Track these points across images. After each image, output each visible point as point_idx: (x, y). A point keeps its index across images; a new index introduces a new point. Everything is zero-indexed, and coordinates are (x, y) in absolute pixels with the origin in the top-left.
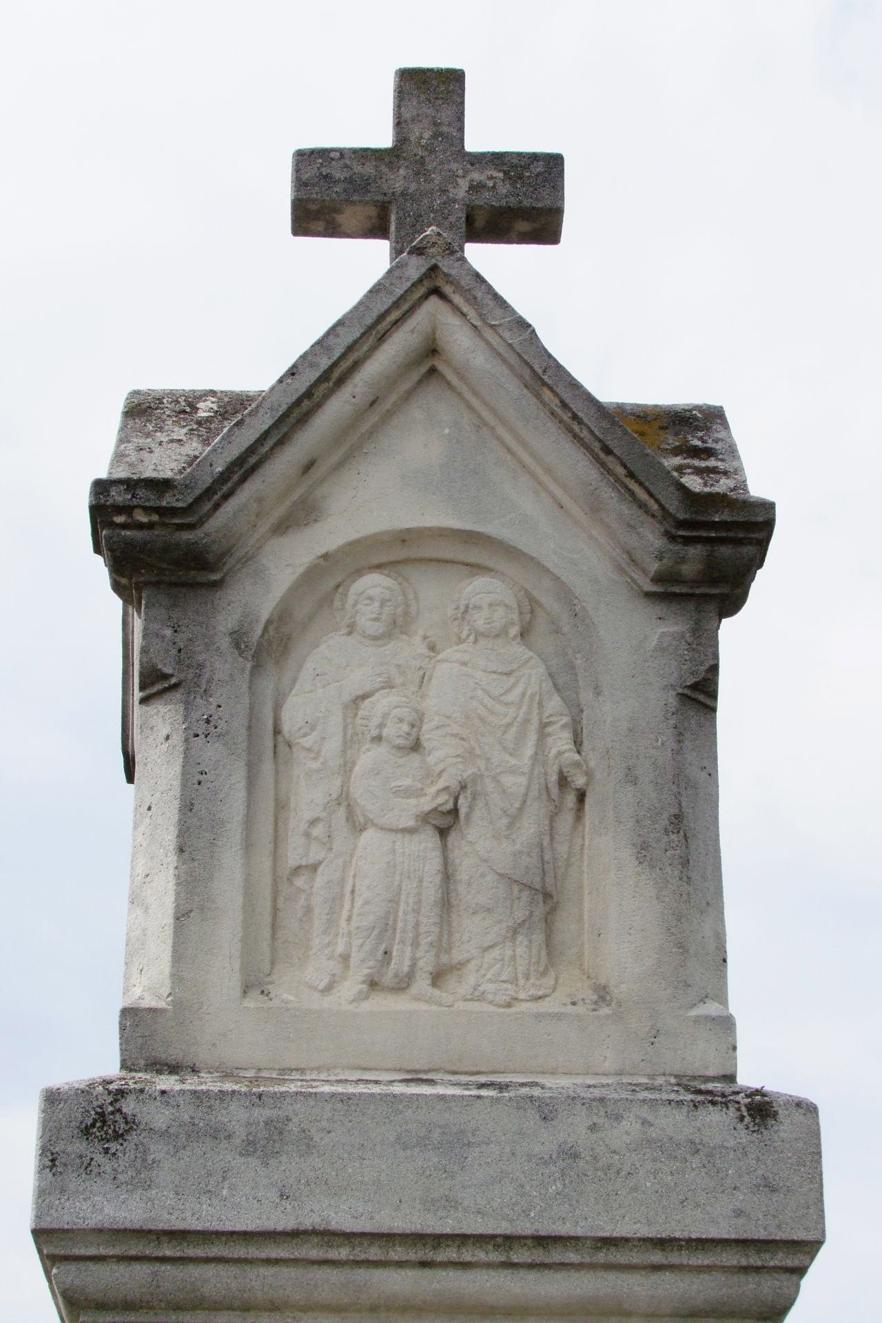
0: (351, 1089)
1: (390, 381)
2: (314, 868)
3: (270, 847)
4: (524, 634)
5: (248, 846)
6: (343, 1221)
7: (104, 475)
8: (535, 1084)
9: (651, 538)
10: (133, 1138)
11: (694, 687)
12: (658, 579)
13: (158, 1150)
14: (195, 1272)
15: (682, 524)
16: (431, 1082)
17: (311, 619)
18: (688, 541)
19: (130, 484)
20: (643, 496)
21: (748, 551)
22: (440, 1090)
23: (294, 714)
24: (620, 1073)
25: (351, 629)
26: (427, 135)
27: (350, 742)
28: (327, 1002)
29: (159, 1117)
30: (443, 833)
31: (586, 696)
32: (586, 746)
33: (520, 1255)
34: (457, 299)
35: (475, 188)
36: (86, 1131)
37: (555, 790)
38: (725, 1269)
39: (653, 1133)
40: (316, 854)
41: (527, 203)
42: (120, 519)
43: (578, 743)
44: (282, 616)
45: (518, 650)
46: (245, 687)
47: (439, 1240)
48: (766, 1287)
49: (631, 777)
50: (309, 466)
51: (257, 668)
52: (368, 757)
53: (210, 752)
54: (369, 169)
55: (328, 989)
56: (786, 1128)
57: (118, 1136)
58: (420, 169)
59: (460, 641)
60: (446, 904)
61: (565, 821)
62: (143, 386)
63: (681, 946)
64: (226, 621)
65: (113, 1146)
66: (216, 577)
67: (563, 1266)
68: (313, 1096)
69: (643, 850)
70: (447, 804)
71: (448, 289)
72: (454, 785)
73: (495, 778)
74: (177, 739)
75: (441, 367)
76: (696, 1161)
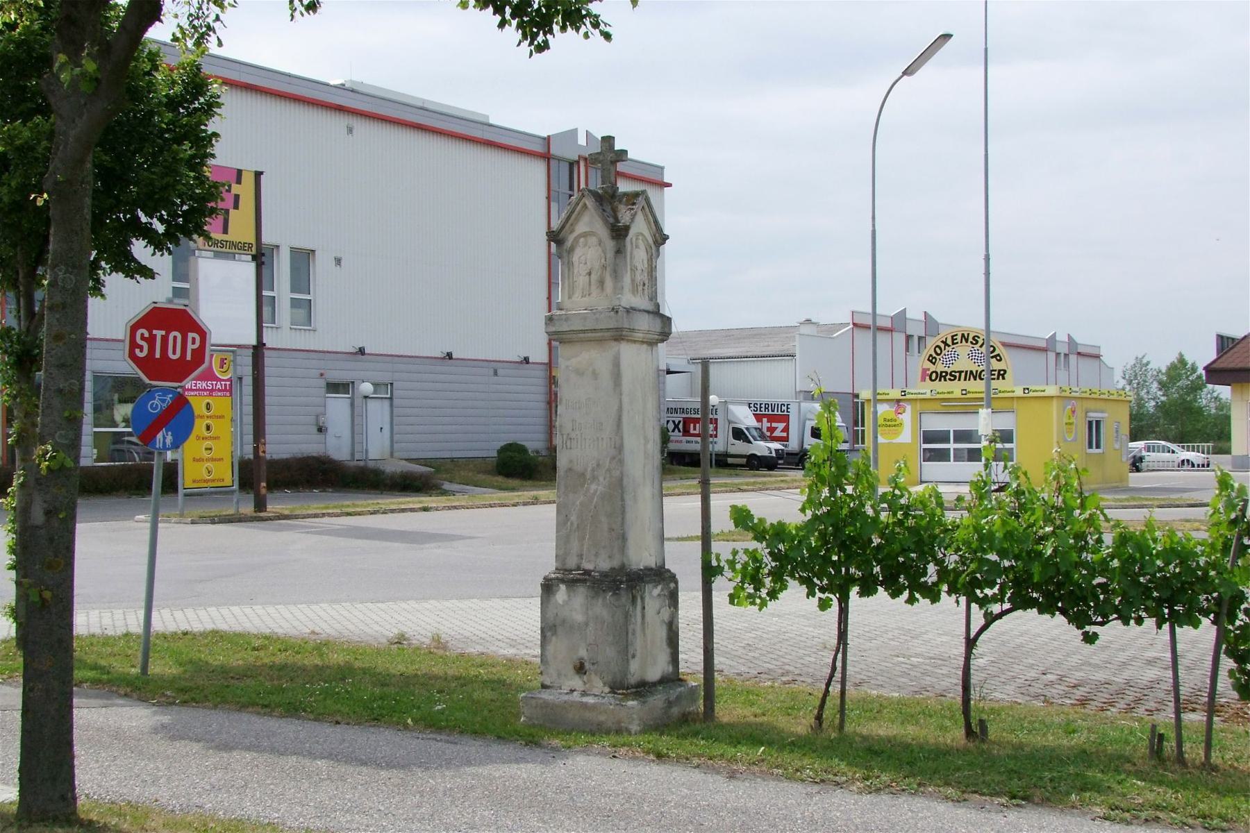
29: (556, 318)
64: (565, 248)
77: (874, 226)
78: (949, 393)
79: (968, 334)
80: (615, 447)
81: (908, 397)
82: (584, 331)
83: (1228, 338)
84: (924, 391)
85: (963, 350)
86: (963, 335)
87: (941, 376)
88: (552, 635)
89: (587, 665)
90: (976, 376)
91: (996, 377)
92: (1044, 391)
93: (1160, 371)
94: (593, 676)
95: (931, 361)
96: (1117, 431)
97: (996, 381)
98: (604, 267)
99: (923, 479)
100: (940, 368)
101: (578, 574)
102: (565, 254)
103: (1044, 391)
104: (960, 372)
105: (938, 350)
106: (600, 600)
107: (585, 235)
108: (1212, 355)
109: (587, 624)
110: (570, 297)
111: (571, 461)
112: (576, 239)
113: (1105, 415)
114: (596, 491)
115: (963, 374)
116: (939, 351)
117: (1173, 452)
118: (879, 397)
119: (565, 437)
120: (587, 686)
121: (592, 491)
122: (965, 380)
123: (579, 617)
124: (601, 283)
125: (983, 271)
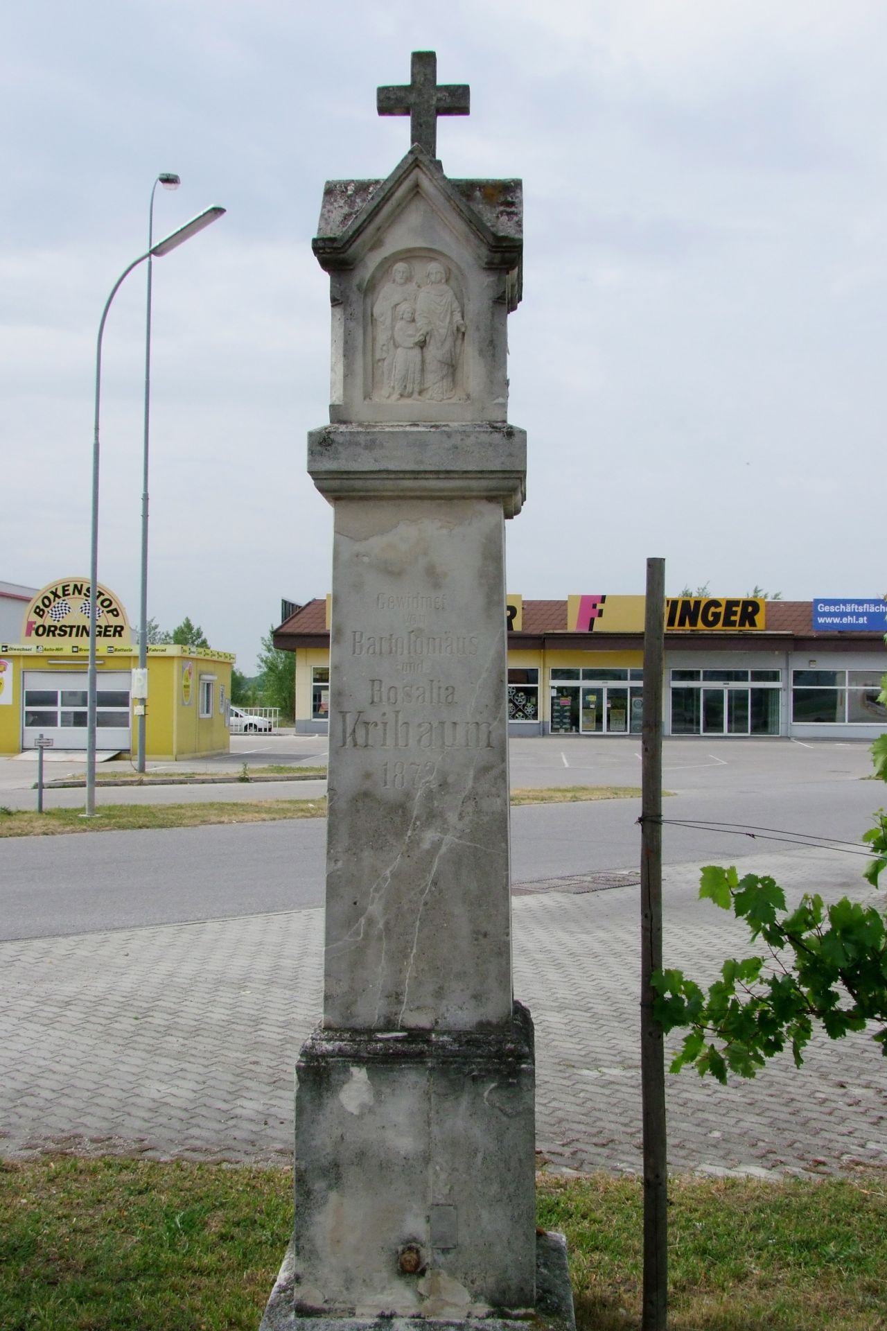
0: (397, 429)
1: (404, 197)
2: (384, 360)
3: (371, 353)
4: (447, 281)
5: (364, 353)
6: (392, 467)
7: (315, 236)
8: (447, 425)
9: (484, 251)
10: (334, 445)
11: (499, 298)
13: (340, 449)
14: (352, 482)
15: (493, 247)
16: (417, 425)
17: (382, 277)
18: (496, 252)
19: (323, 240)
20: (481, 236)
21: (515, 255)
22: (419, 429)
23: (377, 310)
24: (473, 420)
25: (394, 281)
26: (422, 79)
27: (394, 320)
28: (389, 401)
29: (340, 439)
30: (422, 348)
31: (466, 301)
32: (465, 318)
33: (442, 476)
34: (424, 169)
35: (439, 100)
36: (320, 444)
37: (455, 332)
38: (499, 478)
39: (479, 441)
40: (384, 355)
41: (456, 105)
42: (321, 251)
43: (463, 317)
44: (373, 277)
45: (445, 287)
46: (361, 303)
47: (419, 472)
48: (511, 483)
49: (478, 329)
50: (379, 229)
51: (365, 296)
53: (352, 324)
54: (402, 94)
55: (389, 397)
56: (516, 439)
57: (329, 445)
58: (420, 94)
59: (428, 284)
60: (423, 370)
61: (459, 342)
62: (330, 179)
63: (492, 382)
64: (356, 281)
65: (328, 448)
66: (351, 267)
67: (454, 478)
69: (481, 352)
70: (422, 338)
71: (421, 165)
72: (425, 333)
73: (437, 331)
74: (342, 320)
75: (420, 190)
76: (491, 448)
77: (97, 438)
78: (57, 649)
79: (82, 585)
80: (489, 745)
81: (10, 653)
82: (415, 474)
83: (290, 604)
84: (27, 647)
85: (76, 602)
86: (76, 586)
87: (49, 631)
88: (330, 1187)
89: (427, 1256)
90: (82, 630)
91: (112, 633)
92: (164, 650)
93: (168, 635)
94: (444, 1278)
95: (38, 614)
96: (222, 695)
97: (112, 638)
98: (460, 334)
99: (26, 745)
100: (48, 621)
101: (396, 1040)
102: (355, 296)
103: (164, 650)
104: (72, 627)
105: (107, 603)
106: (465, 1101)
107: (408, 255)
108: (277, 623)
109: (427, 1159)
110: (367, 396)
111: (368, 776)
112: (386, 265)
113: (215, 678)
114: (436, 845)
115: (75, 630)
116: (105, 604)
117: (237, 715)
118: (150, 654)
119: (350, 719)
120: (427, 1303)
121: (426, 845)
122: (77, 635)
123: (405, 1143)
124: (452, 367)
125: (140, 512)
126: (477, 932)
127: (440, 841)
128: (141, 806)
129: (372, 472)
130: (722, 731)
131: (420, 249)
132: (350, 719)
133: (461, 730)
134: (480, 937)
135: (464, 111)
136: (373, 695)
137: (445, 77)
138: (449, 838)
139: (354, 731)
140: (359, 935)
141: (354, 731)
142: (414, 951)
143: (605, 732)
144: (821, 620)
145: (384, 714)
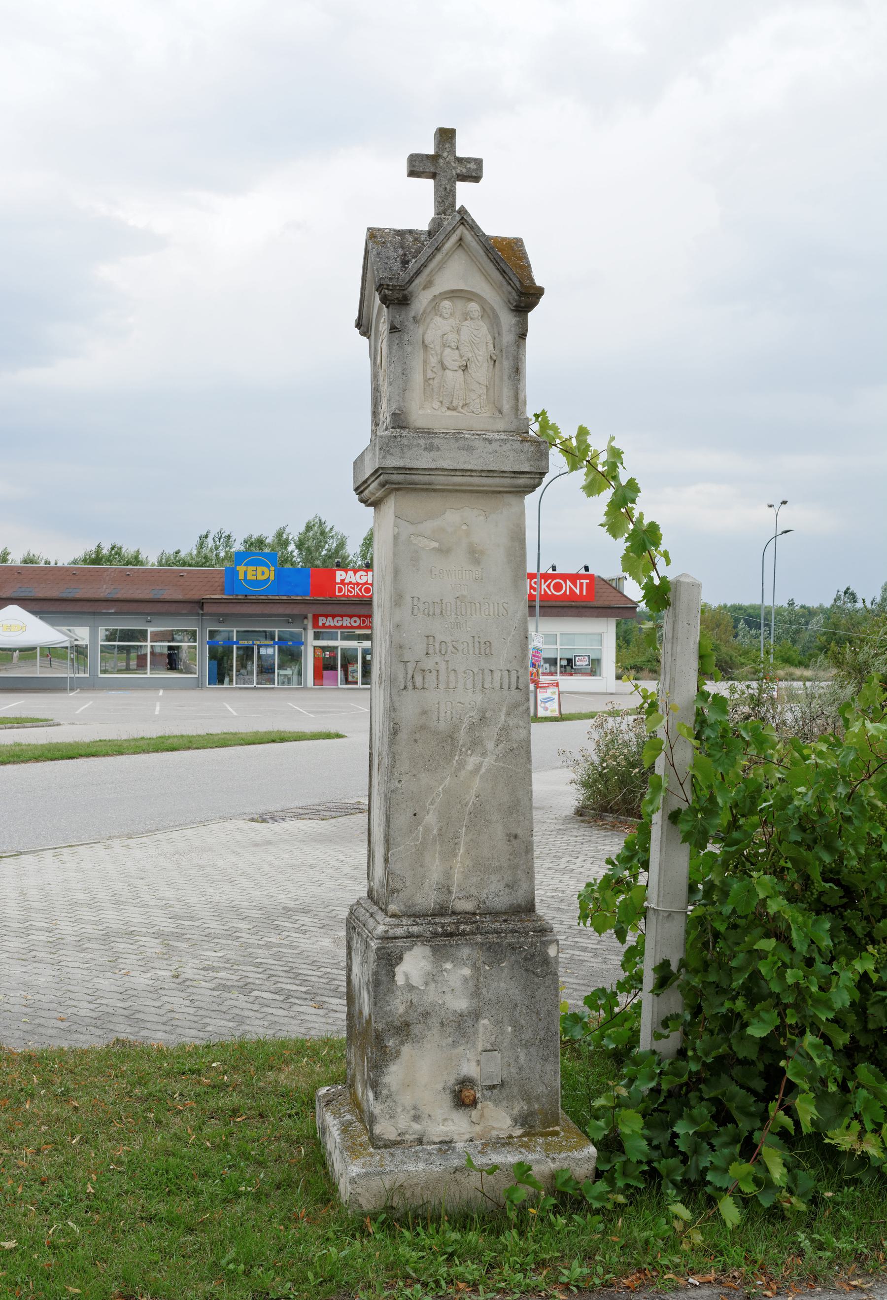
6: (446, 466)
12: (515, 306)
14: (414, 477)
52: (447, 351)
64: (412, 314)
68: (811, 844)
107: (454, 295)
111: (424, 712)
119: (411, 666)
121: (470, 767)
126: (509, 835)
127: (481, 764)
128: (199, 736)
129: (431, 469)
130: (251, 682)
131: (462, 291)
132: (411, 666)
133: (497, 676)
134: (512, 838)
135: (476, 178)
136: (428, 648)
137: (462, 151)
138: (489, 761)
139: (413, 677)
140: (418, 840)
141: (413, 677)
142: (461, 851)
143: (234, 685)
144: (584, 593)
145: (437, 663)
